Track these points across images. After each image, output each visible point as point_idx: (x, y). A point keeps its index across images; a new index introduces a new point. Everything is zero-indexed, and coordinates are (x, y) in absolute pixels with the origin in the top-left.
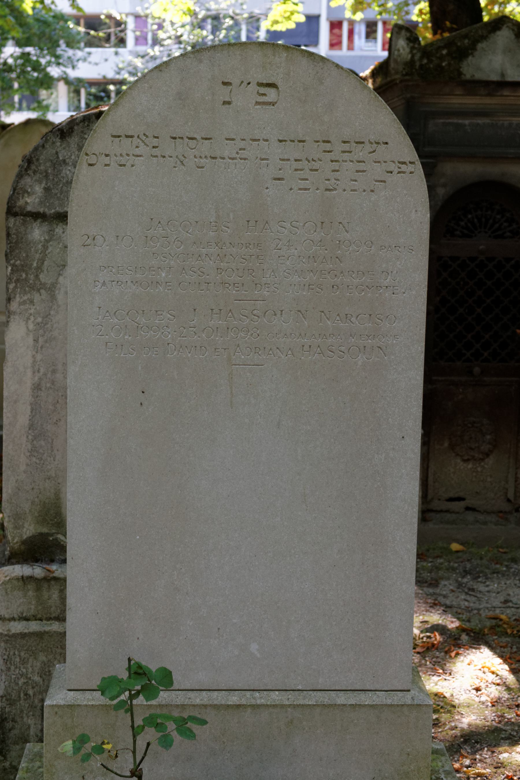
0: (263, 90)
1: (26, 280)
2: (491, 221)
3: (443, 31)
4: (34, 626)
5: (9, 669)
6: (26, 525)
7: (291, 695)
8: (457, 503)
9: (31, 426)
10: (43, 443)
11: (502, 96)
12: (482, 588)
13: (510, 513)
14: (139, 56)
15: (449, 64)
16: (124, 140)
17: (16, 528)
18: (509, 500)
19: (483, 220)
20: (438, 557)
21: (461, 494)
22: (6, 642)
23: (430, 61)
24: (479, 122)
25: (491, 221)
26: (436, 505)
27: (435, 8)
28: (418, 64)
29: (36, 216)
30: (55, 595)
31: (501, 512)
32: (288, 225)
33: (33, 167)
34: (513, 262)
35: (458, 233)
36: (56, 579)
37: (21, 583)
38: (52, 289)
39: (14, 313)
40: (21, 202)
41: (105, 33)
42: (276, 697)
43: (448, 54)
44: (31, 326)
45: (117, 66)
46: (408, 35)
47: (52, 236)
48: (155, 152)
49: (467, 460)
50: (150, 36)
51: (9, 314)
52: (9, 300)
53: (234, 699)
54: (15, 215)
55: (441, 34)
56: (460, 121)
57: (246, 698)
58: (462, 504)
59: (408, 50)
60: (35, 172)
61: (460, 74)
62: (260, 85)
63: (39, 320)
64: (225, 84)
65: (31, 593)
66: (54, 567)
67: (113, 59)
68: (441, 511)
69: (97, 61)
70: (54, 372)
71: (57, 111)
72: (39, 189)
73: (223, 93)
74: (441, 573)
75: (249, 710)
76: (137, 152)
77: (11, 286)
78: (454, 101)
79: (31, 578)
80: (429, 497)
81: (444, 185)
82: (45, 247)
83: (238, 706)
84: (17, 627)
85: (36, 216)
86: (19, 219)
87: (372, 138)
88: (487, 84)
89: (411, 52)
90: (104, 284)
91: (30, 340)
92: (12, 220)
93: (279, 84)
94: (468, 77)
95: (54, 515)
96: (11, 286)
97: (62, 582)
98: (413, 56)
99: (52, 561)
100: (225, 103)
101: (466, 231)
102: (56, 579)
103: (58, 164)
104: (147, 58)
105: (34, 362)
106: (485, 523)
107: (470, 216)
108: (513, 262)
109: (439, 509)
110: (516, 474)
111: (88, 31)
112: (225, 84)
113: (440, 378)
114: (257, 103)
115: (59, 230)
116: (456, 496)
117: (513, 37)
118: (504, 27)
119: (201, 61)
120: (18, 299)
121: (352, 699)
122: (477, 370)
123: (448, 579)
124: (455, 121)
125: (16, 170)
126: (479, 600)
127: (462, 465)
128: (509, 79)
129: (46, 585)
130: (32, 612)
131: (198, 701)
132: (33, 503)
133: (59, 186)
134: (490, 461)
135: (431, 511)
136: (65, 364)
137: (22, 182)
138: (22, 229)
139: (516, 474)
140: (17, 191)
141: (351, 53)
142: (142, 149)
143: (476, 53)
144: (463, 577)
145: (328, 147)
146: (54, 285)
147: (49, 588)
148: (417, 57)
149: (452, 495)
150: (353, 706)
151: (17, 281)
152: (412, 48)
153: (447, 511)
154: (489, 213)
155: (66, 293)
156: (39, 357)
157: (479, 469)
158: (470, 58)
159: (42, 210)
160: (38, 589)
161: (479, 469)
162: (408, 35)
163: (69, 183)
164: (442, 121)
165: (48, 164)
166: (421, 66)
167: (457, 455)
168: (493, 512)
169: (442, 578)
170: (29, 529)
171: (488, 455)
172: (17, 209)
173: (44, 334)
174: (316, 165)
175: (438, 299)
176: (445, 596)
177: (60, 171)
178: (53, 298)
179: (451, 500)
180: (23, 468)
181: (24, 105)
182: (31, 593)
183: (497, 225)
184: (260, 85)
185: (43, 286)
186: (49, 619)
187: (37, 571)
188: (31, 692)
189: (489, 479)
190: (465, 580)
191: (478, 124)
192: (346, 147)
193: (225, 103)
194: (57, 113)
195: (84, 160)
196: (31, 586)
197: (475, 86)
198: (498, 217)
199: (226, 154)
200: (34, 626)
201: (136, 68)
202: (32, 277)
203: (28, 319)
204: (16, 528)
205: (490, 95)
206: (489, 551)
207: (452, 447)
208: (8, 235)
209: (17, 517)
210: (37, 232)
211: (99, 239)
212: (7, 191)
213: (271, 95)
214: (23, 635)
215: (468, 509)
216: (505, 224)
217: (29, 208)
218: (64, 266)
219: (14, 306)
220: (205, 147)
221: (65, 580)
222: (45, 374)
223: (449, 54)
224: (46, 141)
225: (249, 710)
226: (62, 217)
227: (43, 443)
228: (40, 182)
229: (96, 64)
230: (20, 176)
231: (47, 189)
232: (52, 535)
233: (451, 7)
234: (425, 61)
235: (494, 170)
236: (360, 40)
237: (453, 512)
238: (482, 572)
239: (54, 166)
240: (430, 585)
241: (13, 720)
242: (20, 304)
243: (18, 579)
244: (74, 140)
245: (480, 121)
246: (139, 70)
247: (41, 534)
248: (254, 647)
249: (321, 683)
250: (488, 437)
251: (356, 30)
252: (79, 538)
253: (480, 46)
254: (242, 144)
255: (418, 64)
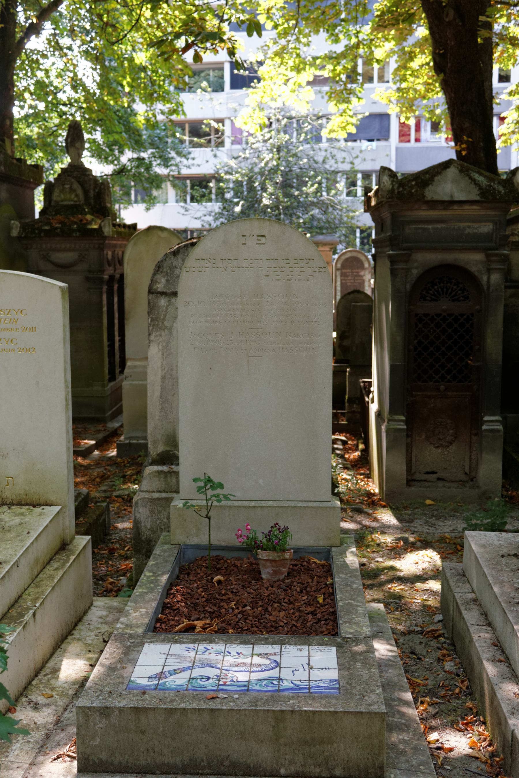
0: (259, 238)
1: (158, 325)
2: (450, 290)
3: (462, 144)
4: (164, 495)
5: (152, 516)
6: (159, 446)
7: (278, 503)
8: (431, 475)
9: (161, 397)
10: (167, 405)
11: (453, 209)
12: (441, 524)
13: (467, 482)
14: (234, 157)
15: (417, 191)
16: (201, 261)
17: (154, 447)
18: (466, 474)
19: (445, 289)
20: (416, 508)
21: (434, 470)
22: (151, 502)
23: (404, 189)
24: (439, 226)
25: (450, 290)
26: (417, 476)
27: (455, 126)
28: (396, 191)
29: (162, 293)
30: (174, 480)
31: (461, 481)
32: (271, 295)
33: (161, 270)
34: (465, 317)
35: (428, 298)
36: (174, 472)
37: (157, 474)
38: (170, 329)
39: (152, 341)
40: (155, 287)
41: (206, 140)
42: (271, 503)
43: (416, 184)
44: (160, 348)
45: (216, 166)
46: (390, 173)
47: (170, 304)
48: (214, 265)
49: (437, 447)
50: (244, 139)
51: (150, 341)
52: (150, 335)
53: (252, 504)
54: (152, 293)
55: (460, 145)
56: (426, 226)
57: (258, 504)
58: (435, 476)
59: (390, 183)
60: (161, 272)
61: (424, 197)
62: (258, 236)
63: (164, 344)
64: (243, 236)
65: (162, 479)
66: (173, 467)
67: (213, 160)
68: (421, 481)
69: (199, 163)
70: (172, 370)
71: (167, 202)
72: (163, 280)
73: (243, 240)
74: (416, 516)
75: (259, 509)
76: (206, 265)
77: (151, 328)
78: (421, 214)
79: (162, 471)
80: (413, 471)
81: (417, 268)
82: (167, 309)
83: (254, 507)
84: (156, 495)
85: (162, 293)
86: (154, 295)
87: (307, 257)
88: (443, 202)
89: (392, 183)
90: (193, 322)
91: (160, 354)
92: (151, 296)
93: (266, 235)
94: (429, 198)
95: (172, 441)
96: (151, 328)
97: (177, 473)
98: (393, 186)
99: (172, 464)
100: (243, 244)
101: (433, 297)
102: (174, 472)
103: (173, 268)
104: (240, 159)
105: (162, 365)
106: (449, 487)
107: (436, 287)
108: (465, 317)
109: (419, 479)
110: (470, 456)
111: (192, 139)
112: (243, 236)
113: (418, 393)
114: (257, 244)
115: (173, 300)
116: (431, 470)
117: (458, 172)
118: (452, 166)
119: (233, 227)
120: (154, 334)
121: (304, 504)
122: (442, 387)
123: (421, 519)
124: (423, 226)
125: (152, 271)
126: (436, 529)
127: (434, 450)
128: (456, 199)
129: (169, 475)
130: (163, 488)
131: (237, 504)
132: (162, 435)
133: (173, 279)
134: (453, 448)
135: (414, 480)
136: (177, 366)
137: (156, 277)
138: (156, 300)
139: (470, 456)
140: (153, 281)
141: (418, 145)
142: (209, 265)
143: (434, 183)
144: (430, 518)
145: (288, 261)
146: (171, 327)
147: (171, 476)
148: (396, 187)
149: (428, 470)
150: (305, 507)
151: (154, 325)
152: (393, 181)
153: (425, 481)
154: (449, 285)
155: (177, 331)
156: (164, 363)
157: (446, 453)
158: (430, 186)
159: (165, 291)
160: (166, 477)
161: (446, 453)
162: (390, 173)
163: (178, 277)
164: (414, 226)
165: (168, 268)
166: (399, 192)
167: (431, 443)
168: (456, 481)
169: (416, 519)
170: (161, 448)
171: (451, 444)
172: (153, 291)
173: (167, 351)
174: (283, 269)
175: (416, 341)
176: (415, 527)
177: (173, 272)
178: (171, 333)
179: (427, 473)
180: (157, 418)
181: (139, 198)
182: (162, 479)
183: (454, 293)
184: (258, 236)
185: (166, 327)
186: (171, 492)
187: (165, 468)
188: (163, 527)
189: (453, 460)
190: (431, 520)
191: (438, 228)
192: (296, 261)
193: (243, 244)
194: (167, 204)
195: (184, 269)
196: (162, 476)
197: (434, 204)
198: (455, 287)
199: (244, 266)
200: (164, 495)
201: (231, 168)
202: (160, 323)
203: (159, 344)
204: (154, 447)
205: (445, 209)
206: (450, 504)
207: (427, 438)
208: (149, 303)
209: (155, 442)
210: (163, 301)
211: (191, 303)
212: (148, 282)
213: (263, 240)
214: (159, 499)
215: (439, 479)
216: (459, 292)
217: (159, 290)
218: (176, 318)
219: (152, 338)
220: (235, 263)
221: (178, 472)
222: (167, 371)
223: (416, 184)
224: (167, 257)
225: (259, 509)
226: (175, 294)
227: (167, 405)
228: (164, 277)
229: (199, 166)
230: (154, 274)
231: (167, 281)
232: (172, 451)
233: (467, 125)
234: (401, 189)
235: (450, 257)
236: (426, 133)
237: (429, 481)
238: (443, 516)
239: (170, 268)
240: (408, 522)
241: (155, 541)
242: (155, 337)
243: (155, 472)
244: (180, 257)
245: (439, 226)
246: (234, 169)
247: (167, 451)
248: (261, 481)
249: (291, 497)
250: (451, 431)
251: (423, 123)
252: (185, 453)
253: (436, 178)
254: (251, 261)
255: (396, 191)
